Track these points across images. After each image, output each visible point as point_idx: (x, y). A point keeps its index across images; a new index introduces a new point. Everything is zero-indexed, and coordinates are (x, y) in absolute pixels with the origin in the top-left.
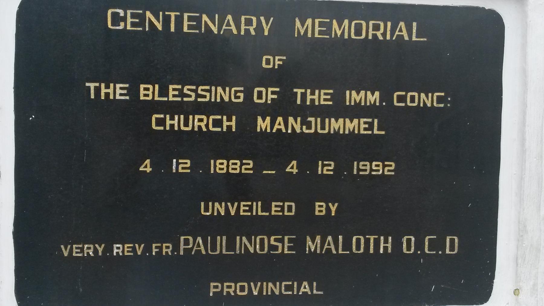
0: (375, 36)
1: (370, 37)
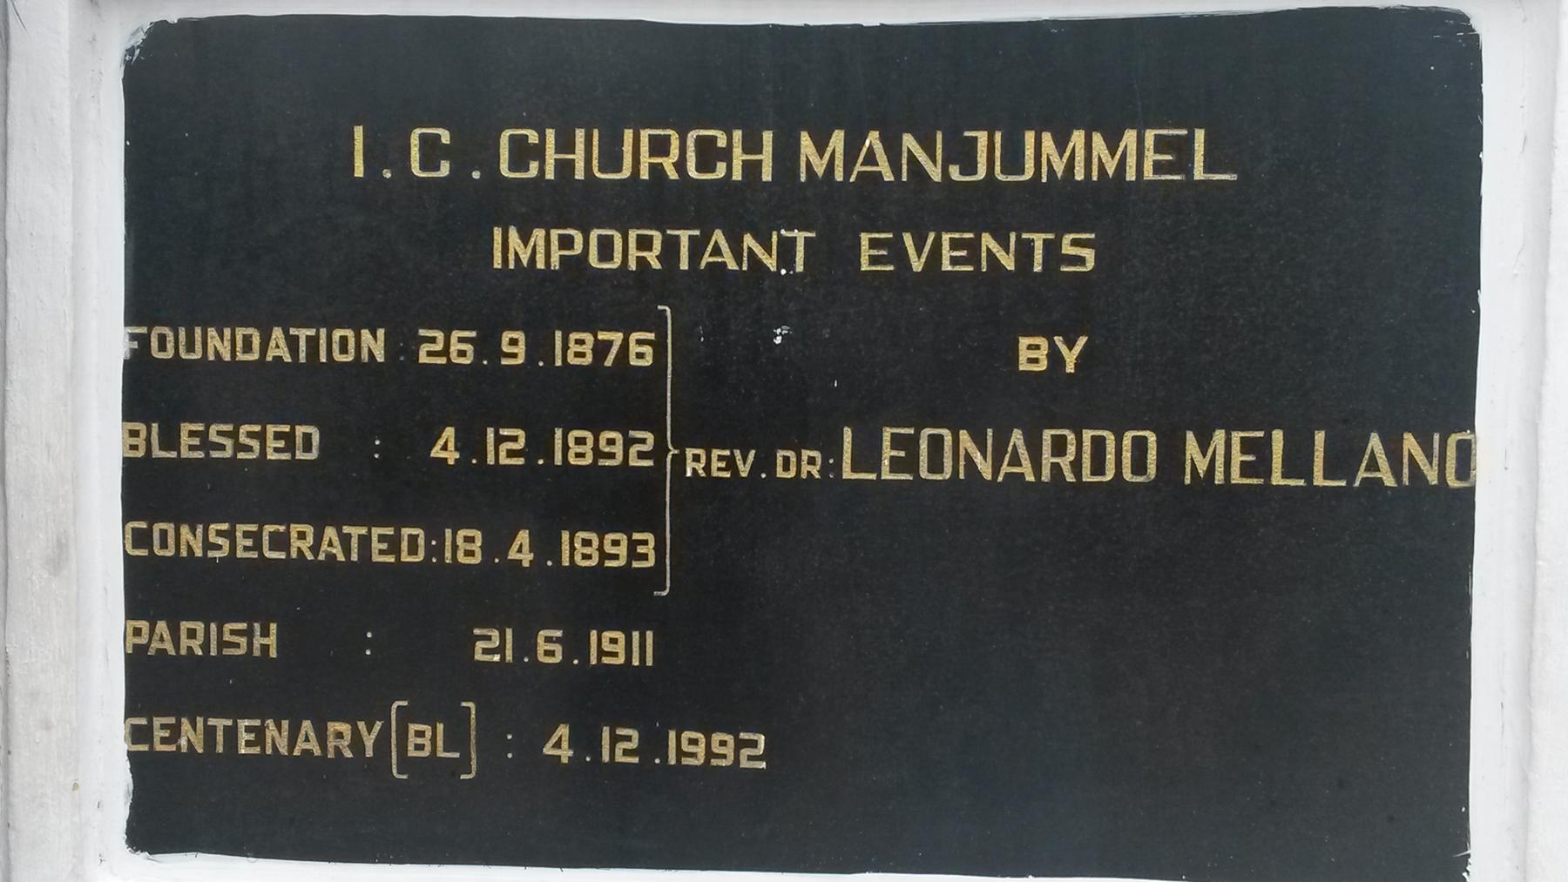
0: (656, 170)
1: (645, 175)
